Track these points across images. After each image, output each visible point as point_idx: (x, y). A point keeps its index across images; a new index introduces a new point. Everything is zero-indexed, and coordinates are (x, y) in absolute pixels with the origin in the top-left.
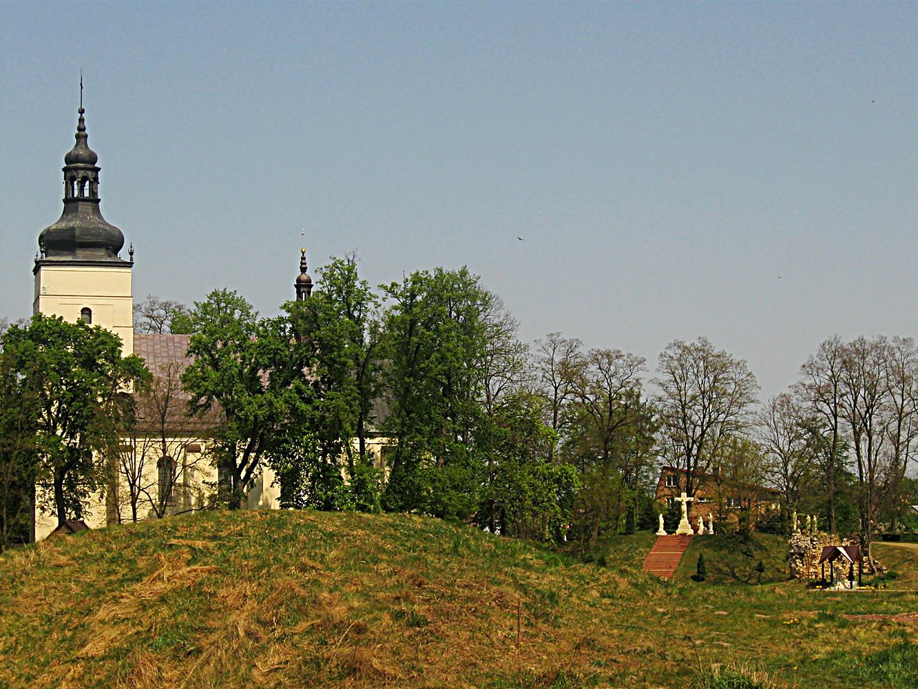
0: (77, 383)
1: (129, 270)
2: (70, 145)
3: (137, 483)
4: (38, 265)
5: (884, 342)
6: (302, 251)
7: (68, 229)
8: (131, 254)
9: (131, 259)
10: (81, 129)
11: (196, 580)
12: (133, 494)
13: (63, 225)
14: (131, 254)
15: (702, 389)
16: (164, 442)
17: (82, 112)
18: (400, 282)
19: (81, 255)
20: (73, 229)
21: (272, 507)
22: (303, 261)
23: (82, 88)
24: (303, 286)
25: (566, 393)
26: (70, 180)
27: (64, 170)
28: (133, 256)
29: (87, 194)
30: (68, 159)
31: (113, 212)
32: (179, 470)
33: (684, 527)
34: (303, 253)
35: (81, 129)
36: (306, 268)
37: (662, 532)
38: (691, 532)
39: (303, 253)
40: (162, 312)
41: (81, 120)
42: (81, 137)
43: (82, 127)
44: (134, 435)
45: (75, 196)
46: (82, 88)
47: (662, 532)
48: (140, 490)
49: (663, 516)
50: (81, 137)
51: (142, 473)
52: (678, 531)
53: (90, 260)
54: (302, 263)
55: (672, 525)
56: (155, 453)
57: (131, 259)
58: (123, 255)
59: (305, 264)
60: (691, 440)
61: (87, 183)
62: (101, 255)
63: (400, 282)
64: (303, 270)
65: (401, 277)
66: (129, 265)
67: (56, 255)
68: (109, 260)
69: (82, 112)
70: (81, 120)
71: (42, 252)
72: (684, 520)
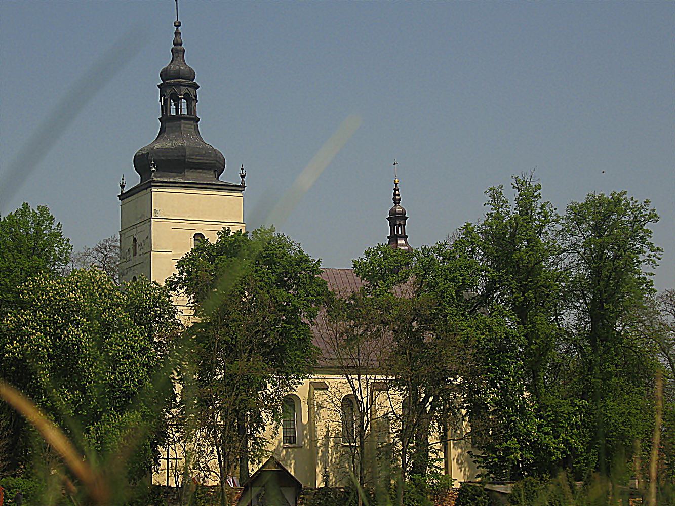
0: (602, 322)
1: (241, 195)
2: (166, 60)
5: (259, 308)
6: (395, 182)
9: (243, 182)
13: (158, 146)
14: (243, 177)
17: (178, 26)
19: (192, 176)
20: (183, 148)
22: (397, 193)
29: (185, 112)
30: (165, 75)
32: (305, 409)
36: (399, 200)
41: (177, 34)
42: (178, 51)
43: (179, 41)
50: (178, 51)
53: (201, 182)
54: (395, 195)
57: (243, 182)
62: (208, 177)
64: (397, 202)
66: (240, 188)
69: (178, 26)
70: (177, 34)
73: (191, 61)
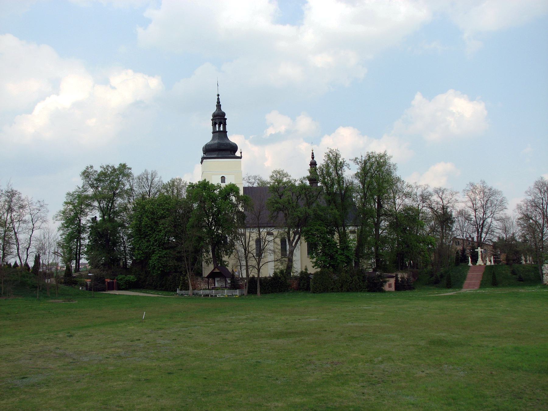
2: (214, 109)
3: (247, 249)
4: (203, 158)
7: (214, 144)
8: (241, 153)
9: (241, 155)
10: (218, 102)
11: (524, 249)
12: (245, 254)
14: (241, 153)
15: (475, 208)
16: (259, 231)
18: (360, 157)
21: (255, 277)
23: (218, 86)
24: (313, 164)
25: (422, 207)
26: (214, 125)
27: (212, 120)
28: (242, 154)
29: (222, 129)
31: (233, 138)
33: (480, 262)
34: (313, 151)
35: (218, 102)
37: (470, 264)
38: (483, 264)
39: (313, 151)
40: (253, 181)
41: (218, 99)
44: (245, 227)
45: (217, 130)
46: (218, 86)
47: (470, 264)
48: (248, 252)
49: (470, 258)
50: (219, 105)
51: (250, 245)
52: (478, 264)
55: (475, 260)
56: (254, 236)
57: (241, 155)
58: (238, 154)
59: (314, 155)
60: (478, 226)
61: (222, 125)
63: (360, 157)
64: (313, 158)
65: (362, 155)
66: (240, 158)
67: (209, 155)
68: (232, 156)
70: (218, 99)
71: (204, 153)
72: (480, 259)
73: (223, 109)
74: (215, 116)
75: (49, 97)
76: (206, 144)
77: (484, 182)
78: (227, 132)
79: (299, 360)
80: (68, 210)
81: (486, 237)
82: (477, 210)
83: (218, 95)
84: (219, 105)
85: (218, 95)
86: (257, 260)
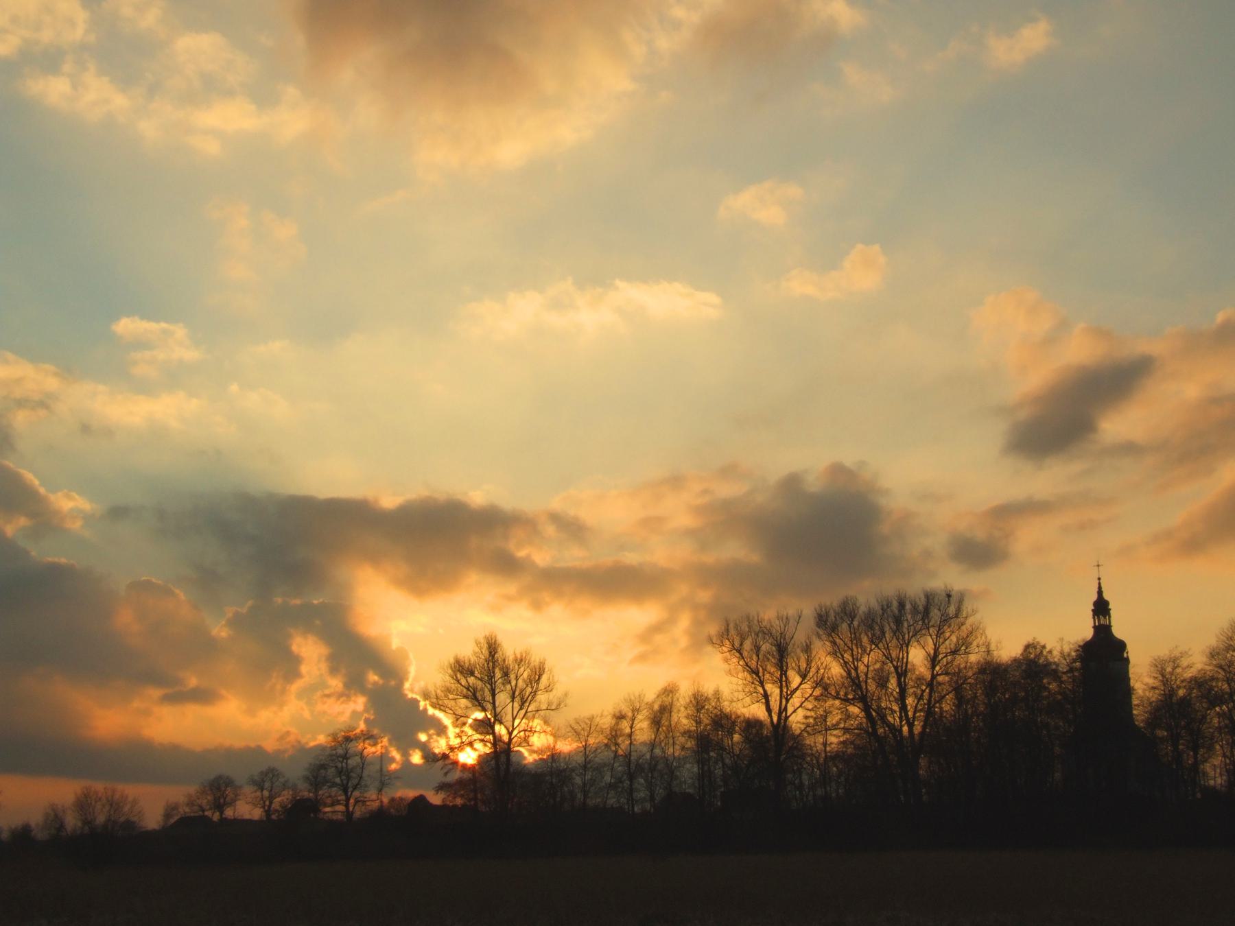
2: (1095, 597)
10: (1100, 588)
35: (1100, 588)
41: (1099, 584)
50: (1100, 592)
70: (1099, 584)
73: (1106, 596)
74: (1095, 604)
75: (1093, 610)
76: (1112, 612)
77: (545, 660)
78: (1110, 609)
79: (476, 677)
80: (519, 668)
81: (802, 686)
82: (352, 774)
83: (1099, 579)
84: (1100, 592)
85: (1099, 579)
86: (935, 640)
